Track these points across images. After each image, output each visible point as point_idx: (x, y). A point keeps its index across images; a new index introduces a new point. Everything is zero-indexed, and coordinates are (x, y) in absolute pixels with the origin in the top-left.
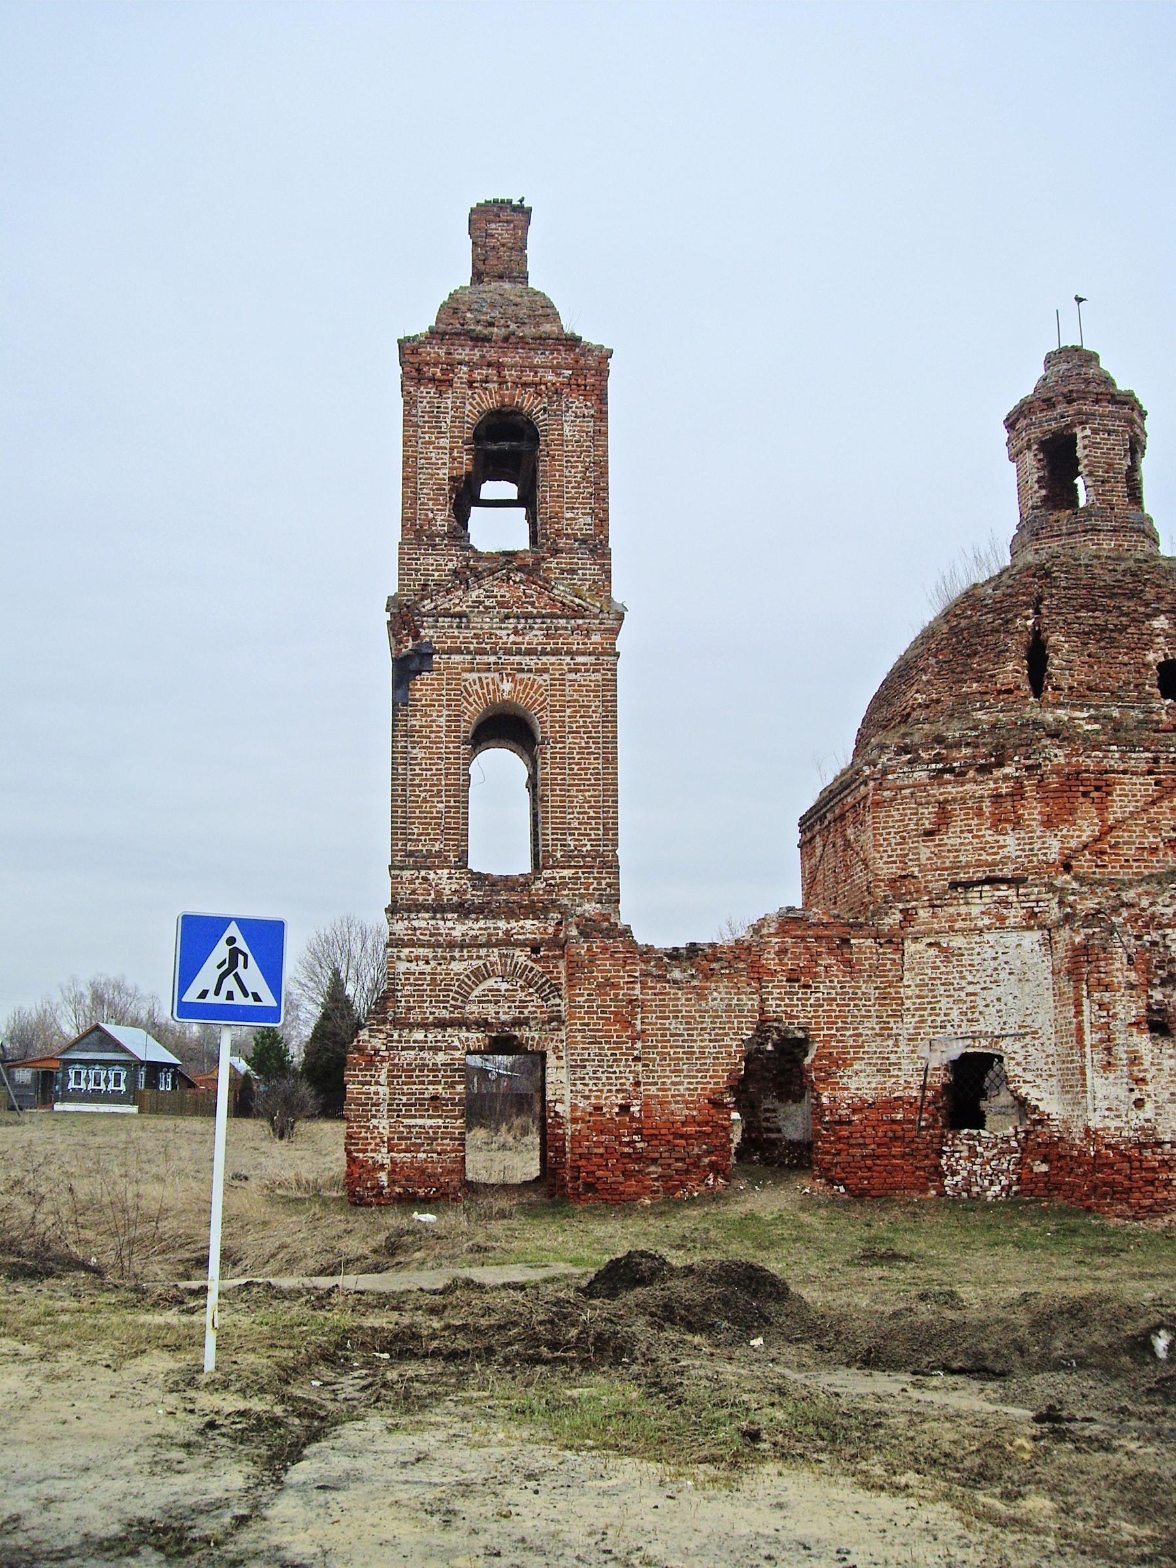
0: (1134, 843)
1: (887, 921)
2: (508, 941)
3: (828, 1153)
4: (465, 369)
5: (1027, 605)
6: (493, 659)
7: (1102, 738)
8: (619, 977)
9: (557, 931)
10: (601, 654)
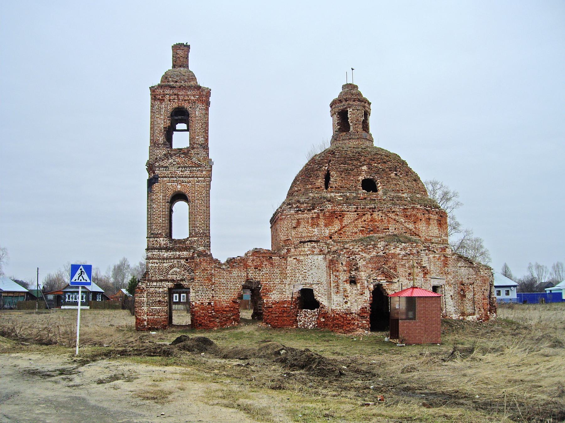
0: (350, 231)
1: (283, 252)
2: (179, 258)
3: (266, 316)
4: (168, 96)
5: (326, 163)
6: (175, 179)
7: (342, 202)
8: (208, 268)
9: (193, 255)
10: (206, 177)
